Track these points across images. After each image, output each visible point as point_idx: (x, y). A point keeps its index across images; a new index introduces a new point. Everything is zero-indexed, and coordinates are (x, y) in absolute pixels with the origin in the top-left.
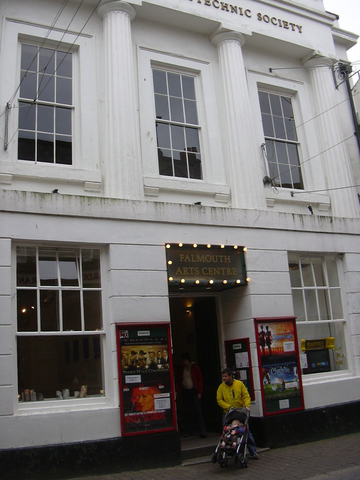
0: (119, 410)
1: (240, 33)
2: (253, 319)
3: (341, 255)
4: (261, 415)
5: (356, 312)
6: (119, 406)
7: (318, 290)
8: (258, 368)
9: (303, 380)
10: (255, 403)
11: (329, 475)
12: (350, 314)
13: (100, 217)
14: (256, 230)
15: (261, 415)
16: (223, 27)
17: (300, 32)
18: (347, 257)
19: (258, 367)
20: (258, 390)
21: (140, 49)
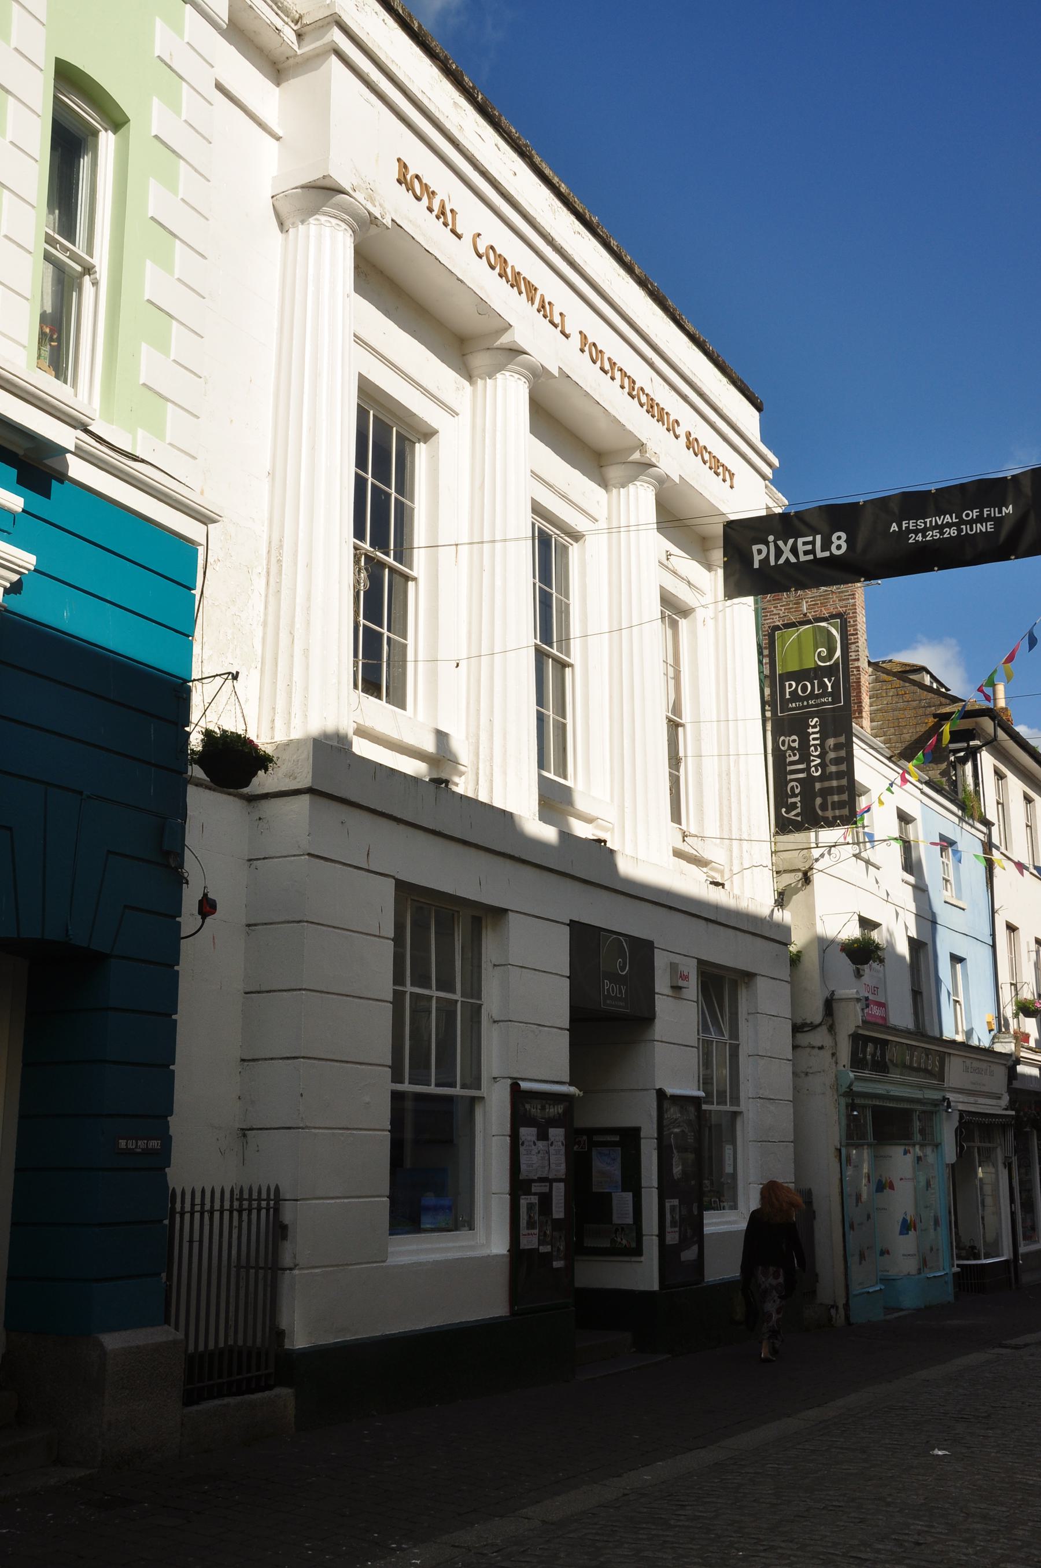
0: (508, 1259)
1: (293, 189)
2: (655, 1091)
3: (499, 913)
4: (656, 1287)
5: (762, 1094)
6: (509, 1251)
7: (429, 987)
8: (656, 1190)
9: (705, 1222)
10: (641, 1262)
11: (1017, 1347)
12: (749, 1098)
13: (410, 822)
14: (689, 918)
15: (656, 1287)
16: (733, 517)
17: (732, 487)
18: (761, 983)
19: (657, 1188)
20: (652, 1235)
21: (355, 341)
